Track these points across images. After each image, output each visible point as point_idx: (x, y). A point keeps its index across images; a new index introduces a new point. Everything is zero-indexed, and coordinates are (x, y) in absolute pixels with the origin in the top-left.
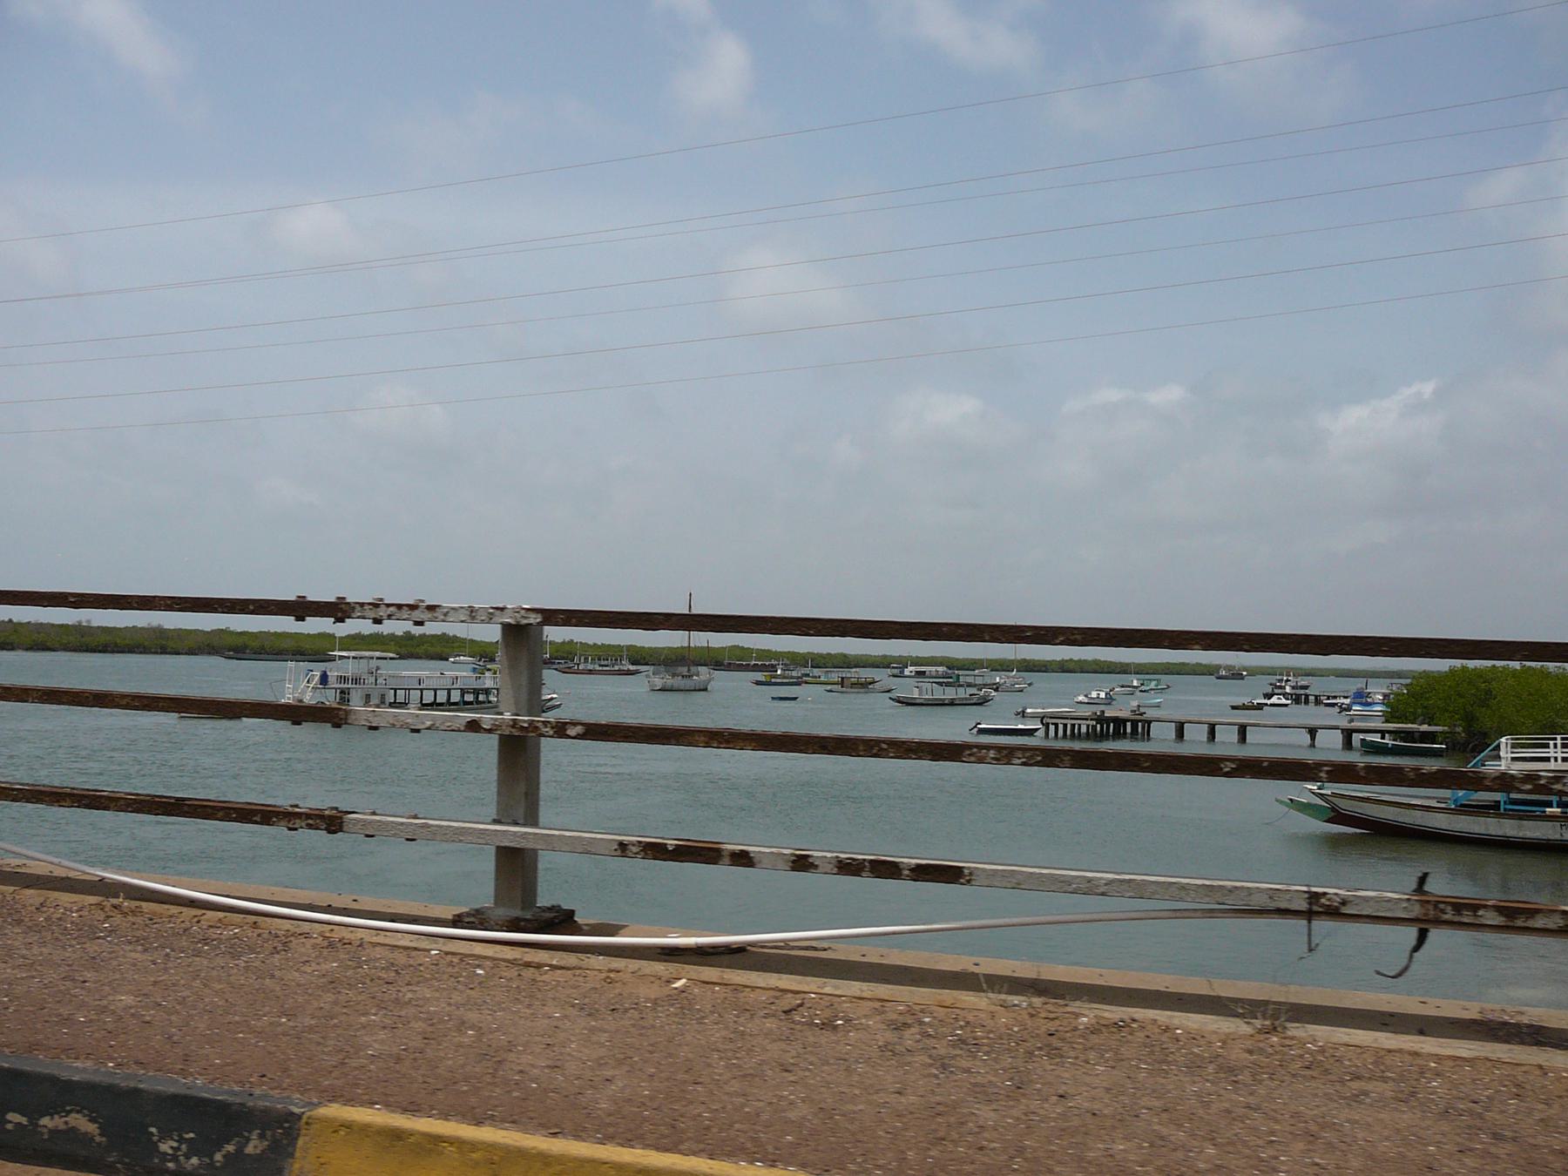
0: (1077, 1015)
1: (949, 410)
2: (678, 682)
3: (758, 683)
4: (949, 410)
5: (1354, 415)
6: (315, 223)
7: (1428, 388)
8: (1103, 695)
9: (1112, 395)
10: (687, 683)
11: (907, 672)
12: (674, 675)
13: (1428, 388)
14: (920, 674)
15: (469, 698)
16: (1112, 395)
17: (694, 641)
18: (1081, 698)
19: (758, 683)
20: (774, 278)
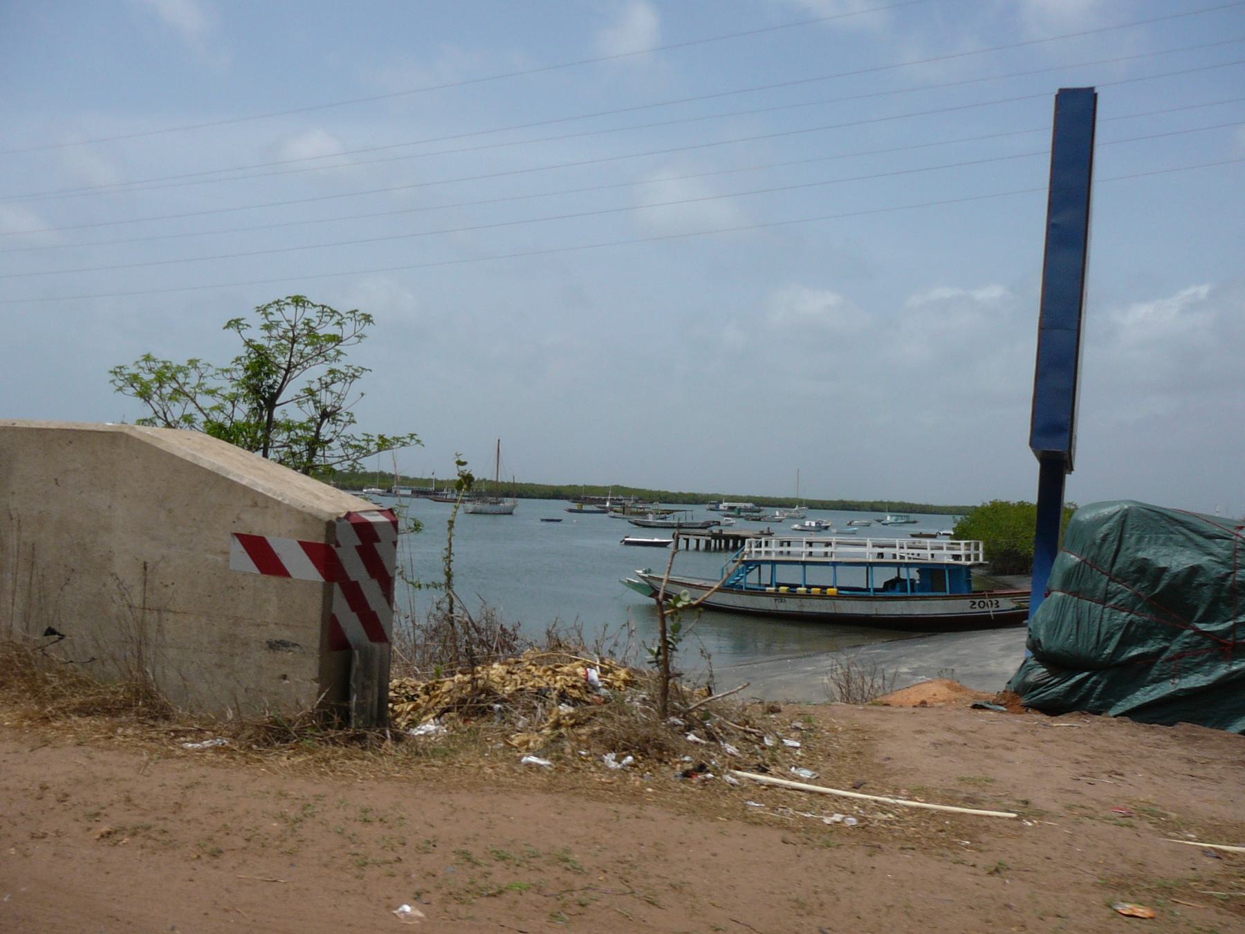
0: (712, 757)
1: (816, 303)
2: (487, 507)
3: (571, 511)
4: (816, 303)
5: (1142, 311)
6: (314, 146)
7: (1204, 290)
8: (813, 524)
9: (946, 292)
10: (495, 508)
11: (721, 507)
12: (484, 502)
13: (1204, 290)
14: (732, 508)
15: (815, 591)
16: (946, 292)
17: (627, 492)
18: (796, 526)
19: (571, 511)
20: (676, 196)
